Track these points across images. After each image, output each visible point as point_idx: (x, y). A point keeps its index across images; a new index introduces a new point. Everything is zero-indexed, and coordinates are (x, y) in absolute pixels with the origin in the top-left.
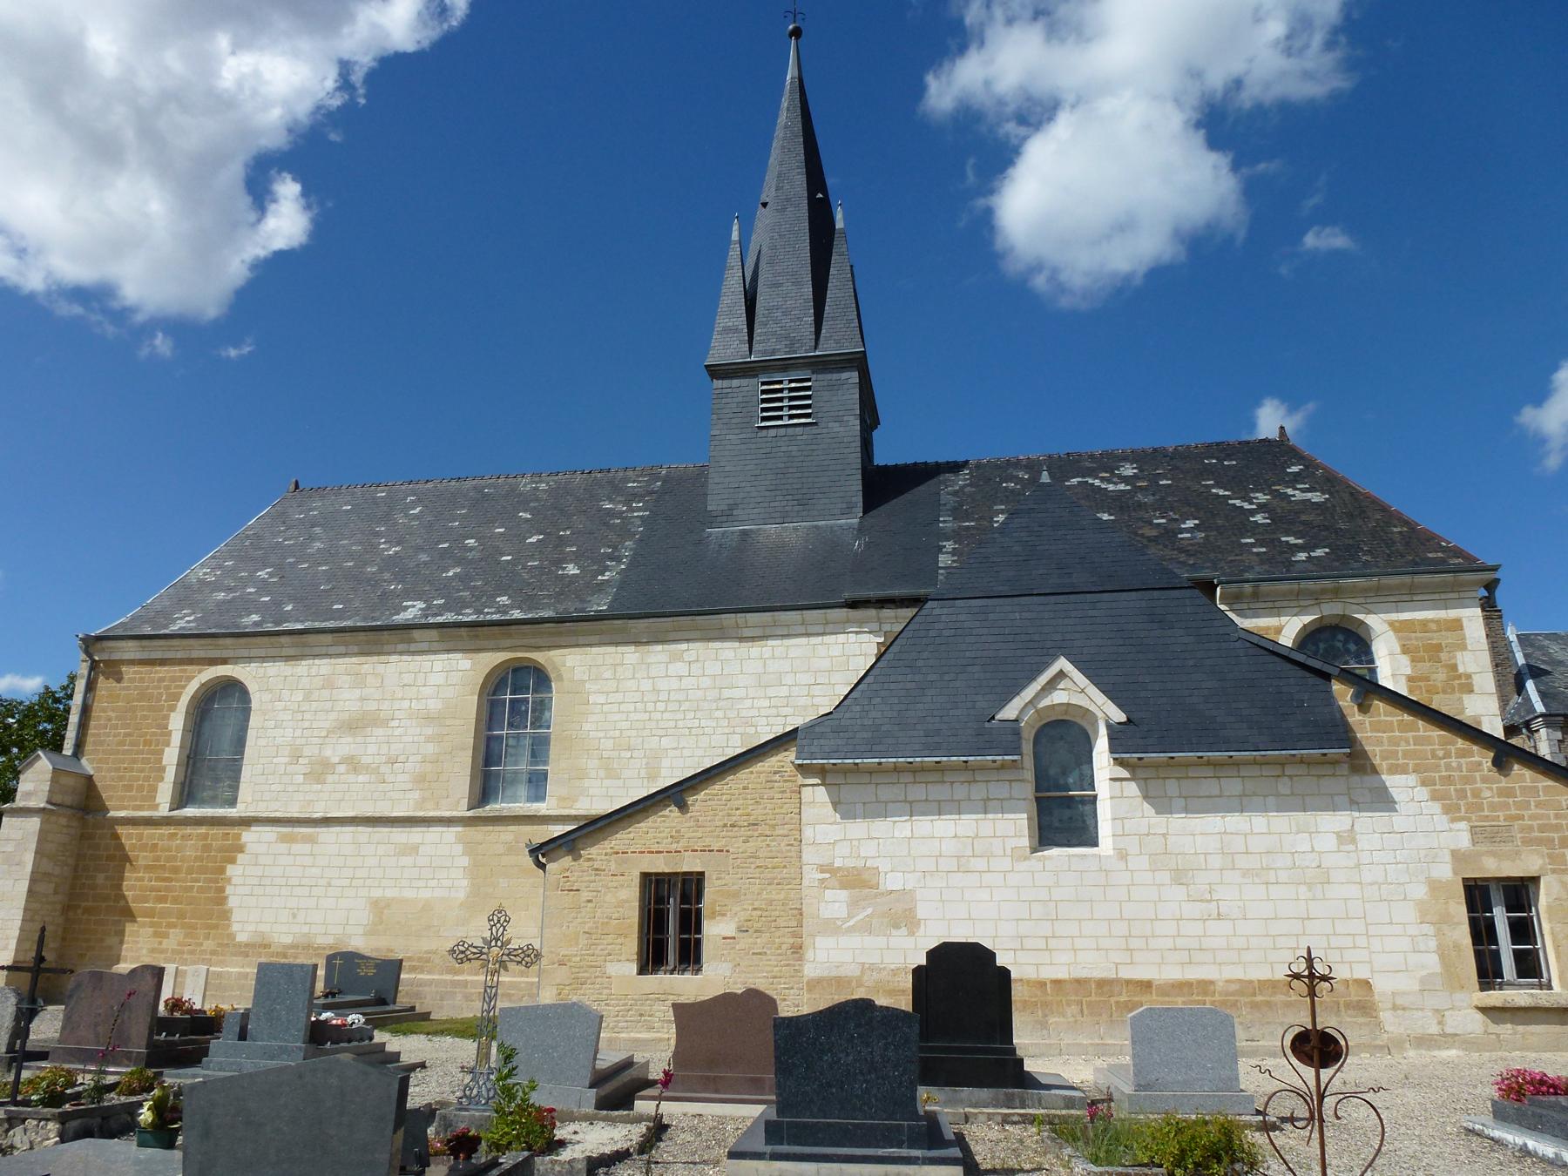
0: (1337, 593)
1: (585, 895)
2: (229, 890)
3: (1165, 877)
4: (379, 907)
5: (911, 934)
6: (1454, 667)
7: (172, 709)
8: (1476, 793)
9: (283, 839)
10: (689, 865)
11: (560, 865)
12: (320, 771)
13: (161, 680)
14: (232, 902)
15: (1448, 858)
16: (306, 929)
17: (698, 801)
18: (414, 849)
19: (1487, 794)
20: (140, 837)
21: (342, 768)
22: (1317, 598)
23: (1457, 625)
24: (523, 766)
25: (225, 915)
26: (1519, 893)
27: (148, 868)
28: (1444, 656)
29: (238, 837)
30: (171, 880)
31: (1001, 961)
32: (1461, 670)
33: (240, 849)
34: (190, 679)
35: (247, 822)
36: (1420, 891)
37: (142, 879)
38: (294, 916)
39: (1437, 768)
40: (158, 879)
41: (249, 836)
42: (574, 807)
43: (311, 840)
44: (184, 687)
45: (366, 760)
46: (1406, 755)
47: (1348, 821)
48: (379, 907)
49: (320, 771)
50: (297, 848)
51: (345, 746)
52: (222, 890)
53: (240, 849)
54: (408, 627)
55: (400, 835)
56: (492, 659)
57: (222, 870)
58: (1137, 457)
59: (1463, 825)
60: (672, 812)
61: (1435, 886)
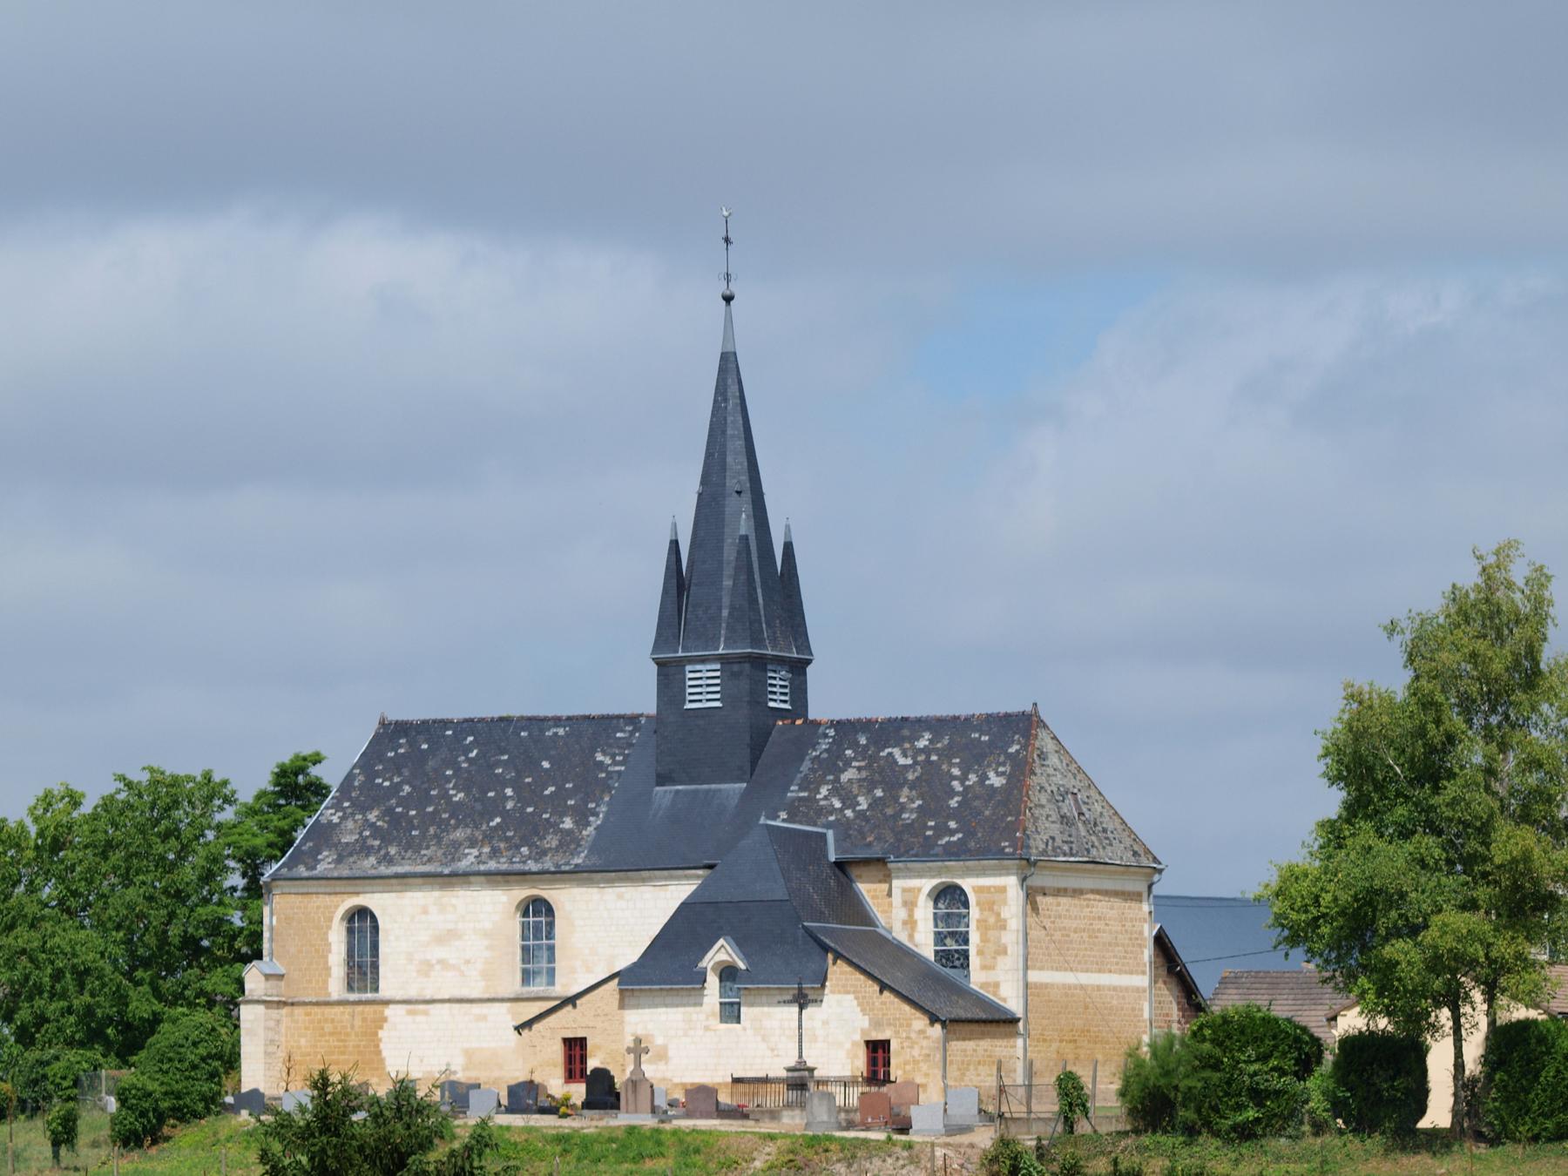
0: (949, 870)
1: (538, 1048)
2: (382, 1046)
3: (759, 1038)
4: (469, 1054)
5: (666, 1063)
6: (999, 915)
7: (329, 928)
8: (873, 1003)
9: (410, 1013)
10: (580, 1034)
11: (525, 1032)
12: (426, 968)
13: (318, 907)
14: (385, 1054)
15: (859, 1031)
16: (429, 1069)
17: (536, 1027)
18: (484, 1018)
19: (877, 1004)
20: (323, 1014)
21: (438, 967)
22: (939, 875)
23: (1002, 890)
24: (545, 965)
25: (382, 1061)
26: (885, 1045)
27: (331, 1034)
28: (995, 907)
29: (382, 1012)
30: (345, 1041)
31: (612, 1073)
32: (1002, 916)
33: (385, 1020)
34: (337, 907)
35: (387, 1002)
36: (848, 1046)
37: (328, 1041)
38: (422, 1061)
39: (861, 992)
40: (338, 1041)
41: (390, 1011)
42: (222, 1136)
43: (426, 1013)
44: (334, 912)
45: (452, 962)
46: (852, 986)
47: (9, 1128)
48: (469, 1054)
49: (426, 968)
50: (420, 1018)
51: (439, 953)
52: (378, 1046)
53: (385, 1020)
54: (466, 874)
55: (476, 1009)
56: (522, 893)
57: (376, 1034)
58: (937, 725)
59: (867, 1017)
60: (569, 1008)
61: (854, 1044)
